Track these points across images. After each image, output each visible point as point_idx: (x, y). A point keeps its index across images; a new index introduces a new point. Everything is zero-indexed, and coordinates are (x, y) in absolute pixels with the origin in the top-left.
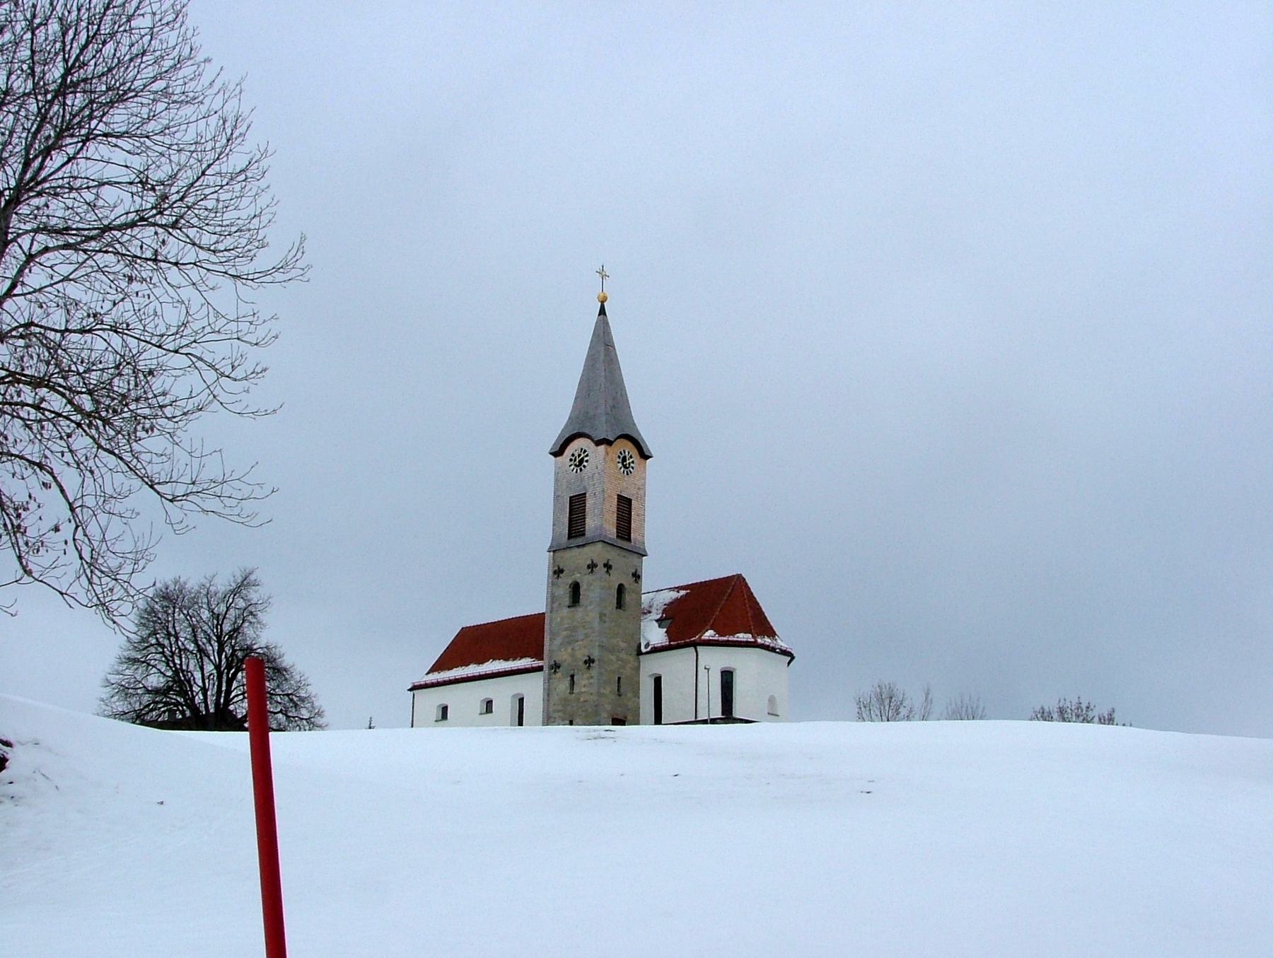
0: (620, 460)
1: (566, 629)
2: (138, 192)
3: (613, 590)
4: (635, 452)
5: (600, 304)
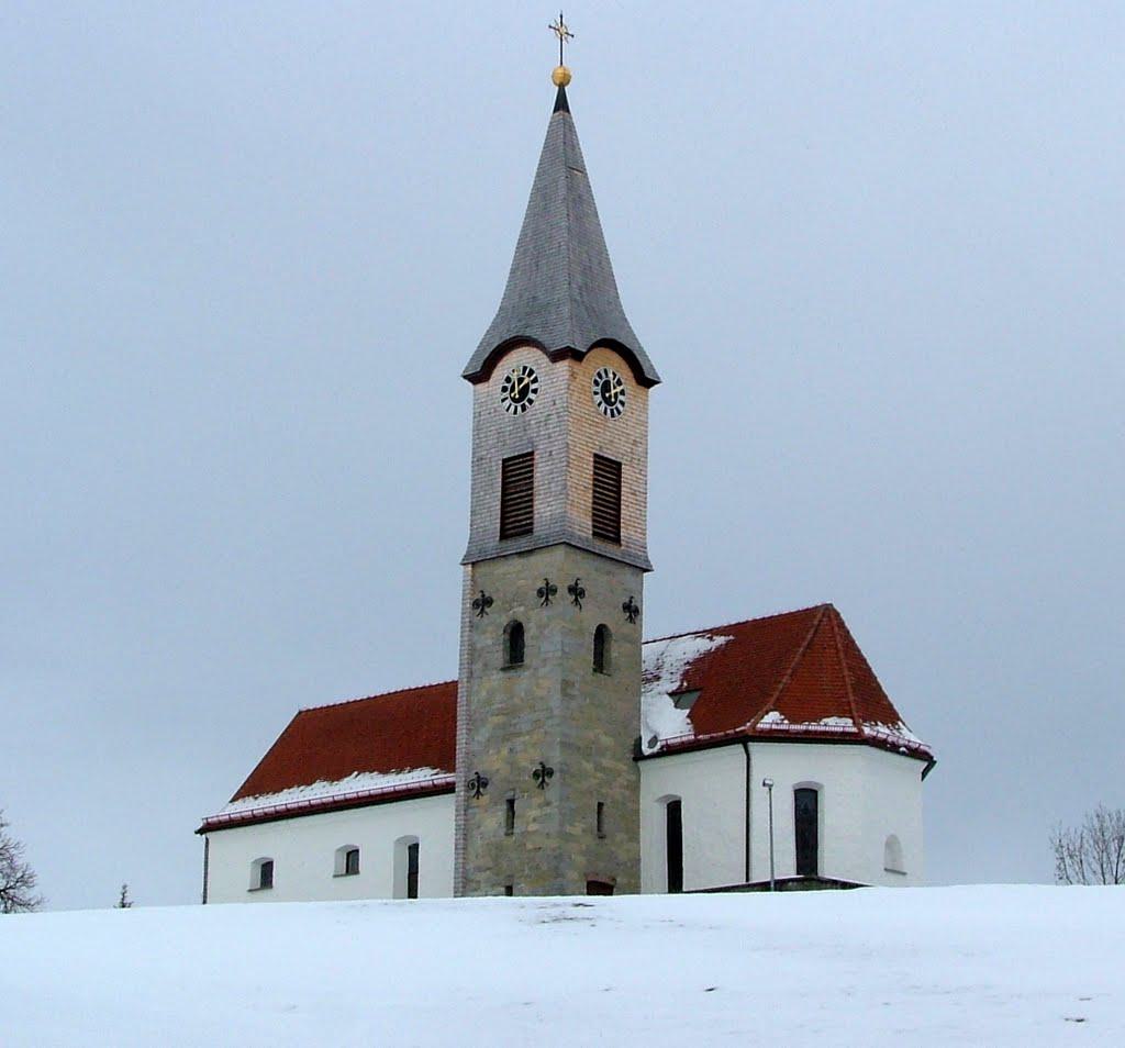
0: (598, 389)
1: (500, 713)
5: (557, 88)
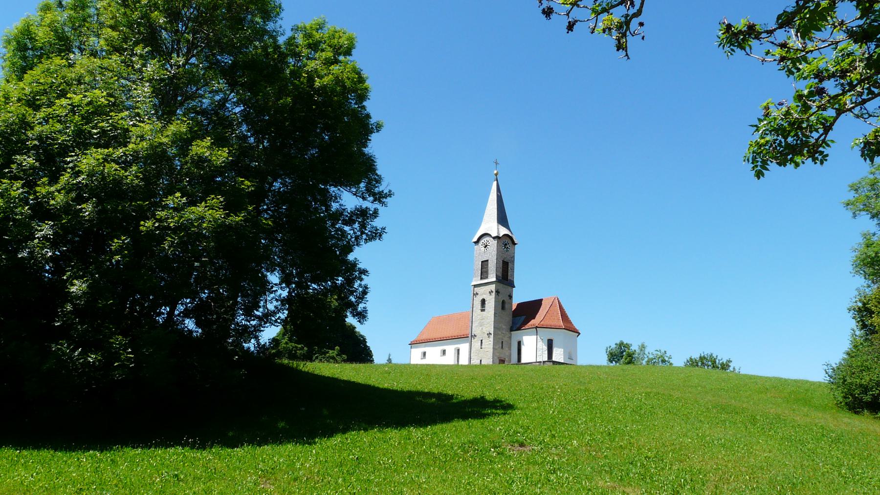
2: (862, 114)
3: (476, 315)
4: (510, 242)
